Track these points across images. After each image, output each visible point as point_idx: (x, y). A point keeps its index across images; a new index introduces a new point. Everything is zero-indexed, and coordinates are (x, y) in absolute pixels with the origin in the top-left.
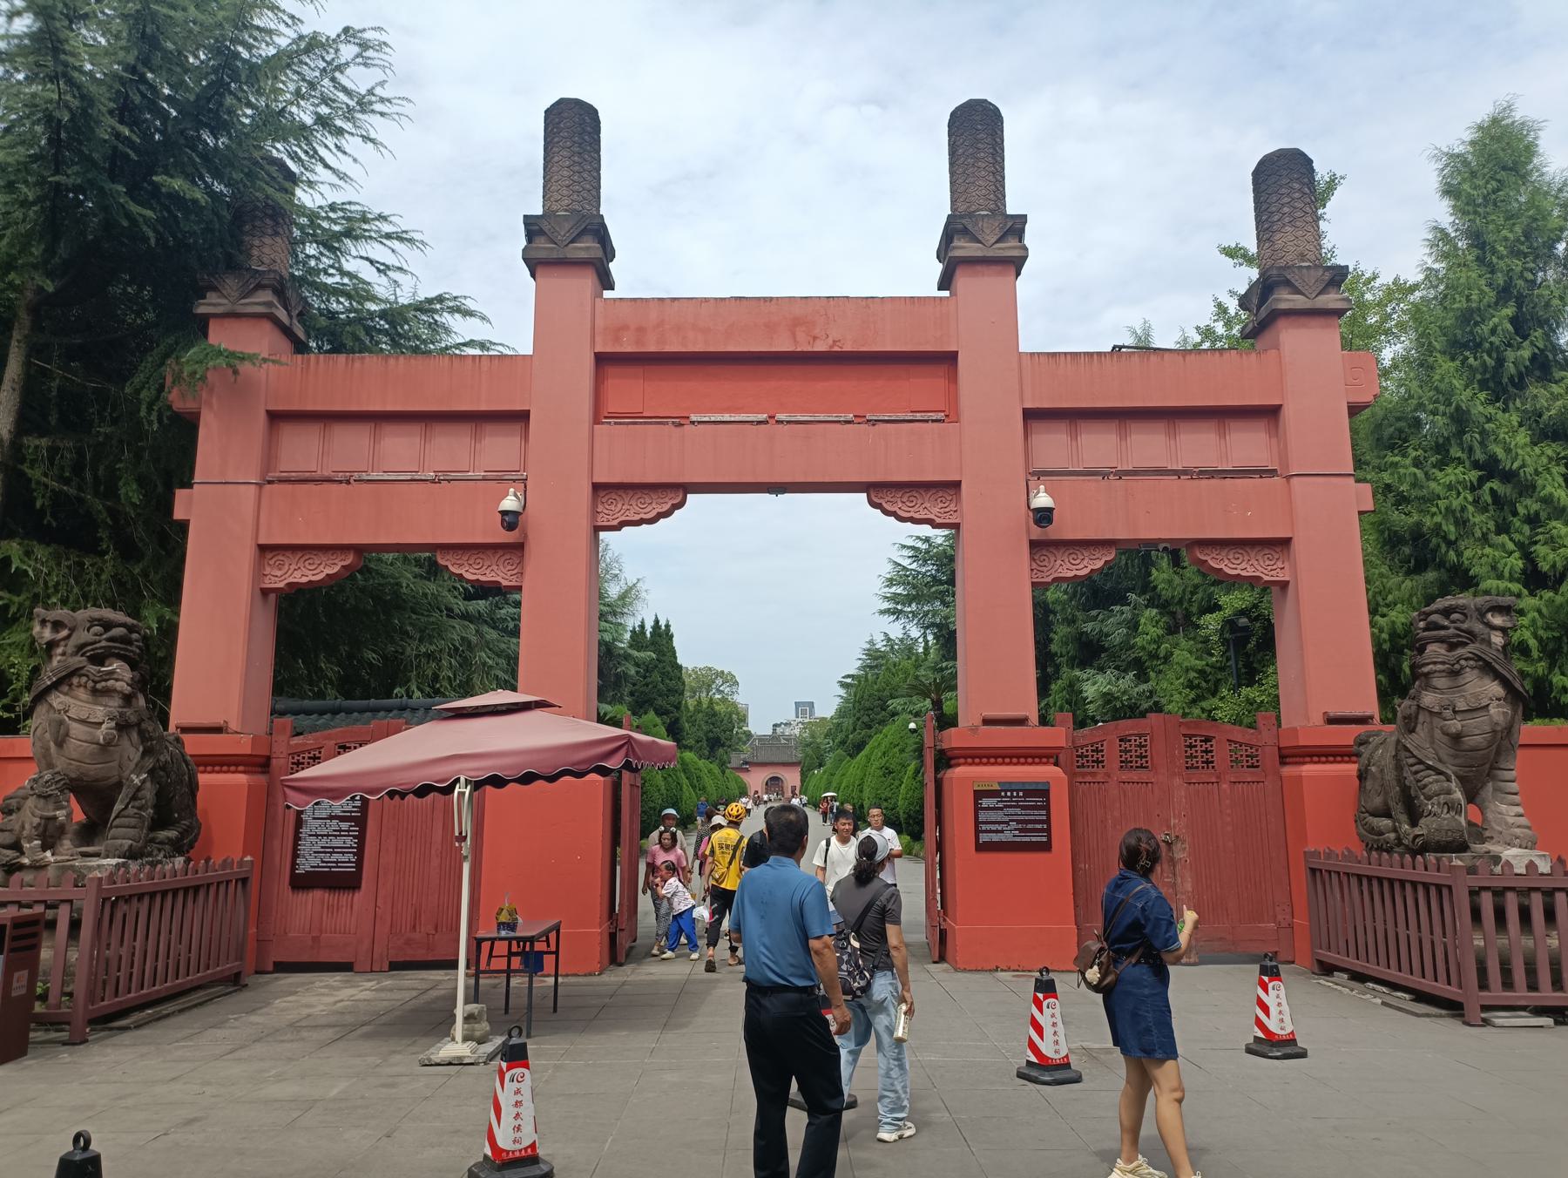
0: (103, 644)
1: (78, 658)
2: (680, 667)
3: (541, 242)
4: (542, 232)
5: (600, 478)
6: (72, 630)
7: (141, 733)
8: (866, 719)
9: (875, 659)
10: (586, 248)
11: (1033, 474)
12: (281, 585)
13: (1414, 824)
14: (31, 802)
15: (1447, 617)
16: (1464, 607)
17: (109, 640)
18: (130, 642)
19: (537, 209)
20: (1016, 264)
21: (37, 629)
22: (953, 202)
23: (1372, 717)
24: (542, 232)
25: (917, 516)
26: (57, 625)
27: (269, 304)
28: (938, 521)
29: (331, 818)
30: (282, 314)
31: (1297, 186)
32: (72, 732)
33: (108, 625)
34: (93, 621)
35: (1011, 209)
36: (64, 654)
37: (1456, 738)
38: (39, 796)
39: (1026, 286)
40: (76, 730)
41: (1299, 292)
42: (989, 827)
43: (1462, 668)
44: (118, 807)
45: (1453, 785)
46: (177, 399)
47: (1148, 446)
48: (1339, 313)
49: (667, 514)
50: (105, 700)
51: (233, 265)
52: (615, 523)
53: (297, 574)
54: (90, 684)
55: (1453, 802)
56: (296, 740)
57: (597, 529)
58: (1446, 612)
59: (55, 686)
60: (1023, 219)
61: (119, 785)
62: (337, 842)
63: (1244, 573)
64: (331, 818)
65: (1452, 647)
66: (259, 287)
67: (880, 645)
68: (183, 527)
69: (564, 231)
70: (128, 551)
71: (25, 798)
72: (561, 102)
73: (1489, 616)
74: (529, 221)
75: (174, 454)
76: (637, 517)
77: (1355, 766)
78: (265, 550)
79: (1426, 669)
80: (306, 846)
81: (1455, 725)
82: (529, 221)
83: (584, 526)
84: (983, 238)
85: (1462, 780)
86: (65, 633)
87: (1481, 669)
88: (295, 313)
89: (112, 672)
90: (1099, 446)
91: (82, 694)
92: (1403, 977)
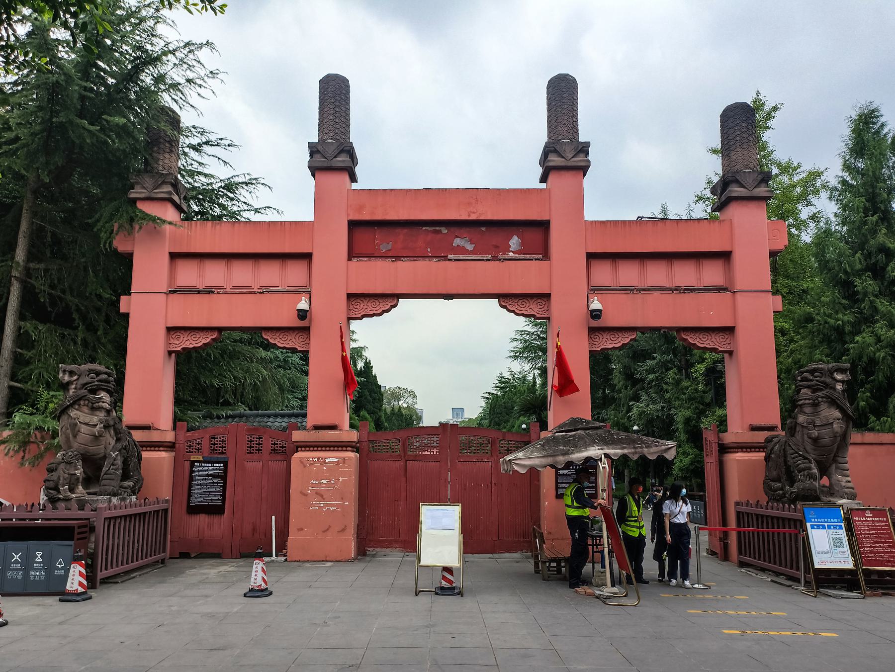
0: (96, 383)
1: (83, 391)
2: (380, 387)
3: (318, 157)
4: (318, 152)
5: (353, 291)
6: (79, 376)
7: (115, 430)
8: (497, 419)
9: (504, 384)
10: (343, 159)
11: (591, 290)
12: (179, 349)
13: (792, 486)
14: (62, 466)
15: (813, 375)
16: (822, 369)
17: (98, 381)
18: (109, 382)
19: (315, 139)
20: (584, 169)
21: (61, 375)
22: (549, 133)
23: (776, 427)
24: (318, 152)
25: (525, 313)
26: (71, 373)
27: (170, 193)
28: (538, 316)
29: (208, 476)
30: (176, 198)
31: (745, 125)
32: (82, 430)
33: (98, 373)
34: (91, 371)
35: (582, 138)
36: (75, 388)
37: (815, 440)
38: (67, 463)
39: (589, 181)
40: (84, 429)
41: (744, 187)
42: (563, 485)
43: (819, 402)
44: (105, 469)
45: (813, 465)
46: (121, 245)
47: (657, 274)
48: (765, 199)
49: (388, 311)
50: (98, 413)
51: (148, 168)
52: (359, 316)
53: (188, 343)
54: (90, 404)
55: (812, 474)
56: (189, 434)
57: (349, 319)
58: (812, 372)
59: (72, 405)
60: (588, 144)
61: (105, 457)
62: (212, 489)
63: (708, 346)
64: (208, 476)
65: (814, 391)
66: (164, 183)
67: (507, 375)
68: (126, 316)
69: (331, 151)
70: (91, 328)
71: (59, 464)
72: (328, 76)
73: (835, 374)
74: (311, 146)
75: (120, 273)
76: (371, 313)
77: (764, 454)
78: (171, 330)
79: (800, 403)
80: (196, 490)
81: (815, 433)
82: (311, 146)
83: (344, 317)
84: (565, 155)
85: (819, 464)
86: (75, 377)
87: (829, 402)
88: (182, 197)
89: (101, 398)
90: (629, 274)
91: (85, 409)
92: (782, 569)
